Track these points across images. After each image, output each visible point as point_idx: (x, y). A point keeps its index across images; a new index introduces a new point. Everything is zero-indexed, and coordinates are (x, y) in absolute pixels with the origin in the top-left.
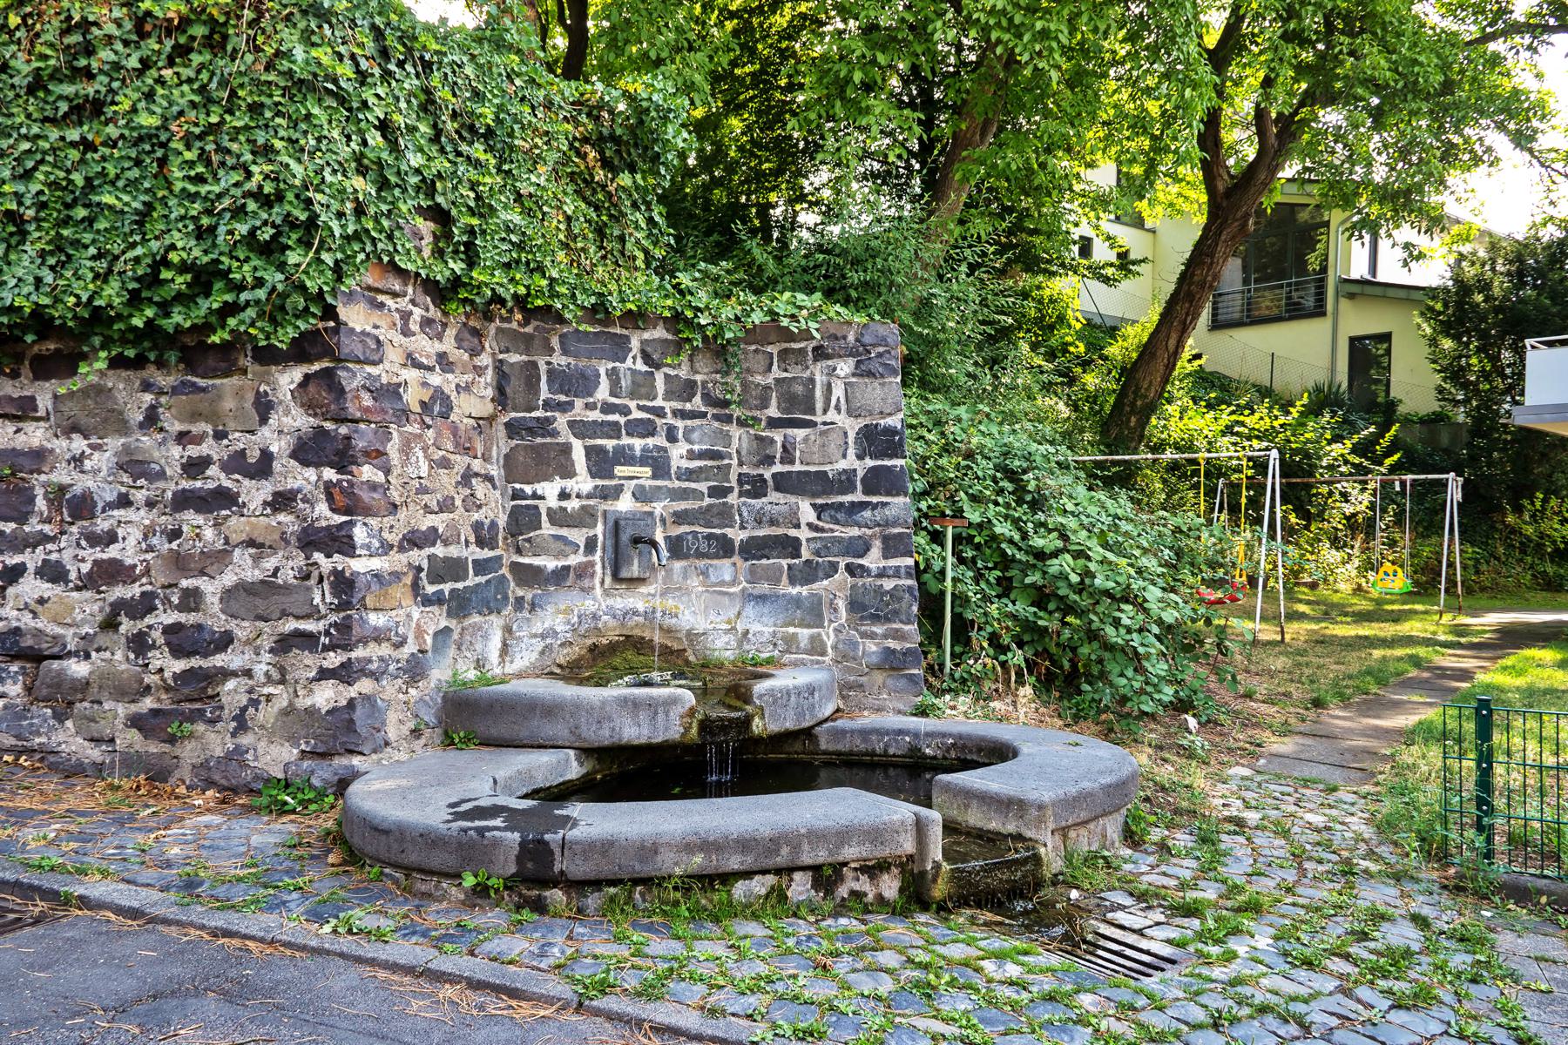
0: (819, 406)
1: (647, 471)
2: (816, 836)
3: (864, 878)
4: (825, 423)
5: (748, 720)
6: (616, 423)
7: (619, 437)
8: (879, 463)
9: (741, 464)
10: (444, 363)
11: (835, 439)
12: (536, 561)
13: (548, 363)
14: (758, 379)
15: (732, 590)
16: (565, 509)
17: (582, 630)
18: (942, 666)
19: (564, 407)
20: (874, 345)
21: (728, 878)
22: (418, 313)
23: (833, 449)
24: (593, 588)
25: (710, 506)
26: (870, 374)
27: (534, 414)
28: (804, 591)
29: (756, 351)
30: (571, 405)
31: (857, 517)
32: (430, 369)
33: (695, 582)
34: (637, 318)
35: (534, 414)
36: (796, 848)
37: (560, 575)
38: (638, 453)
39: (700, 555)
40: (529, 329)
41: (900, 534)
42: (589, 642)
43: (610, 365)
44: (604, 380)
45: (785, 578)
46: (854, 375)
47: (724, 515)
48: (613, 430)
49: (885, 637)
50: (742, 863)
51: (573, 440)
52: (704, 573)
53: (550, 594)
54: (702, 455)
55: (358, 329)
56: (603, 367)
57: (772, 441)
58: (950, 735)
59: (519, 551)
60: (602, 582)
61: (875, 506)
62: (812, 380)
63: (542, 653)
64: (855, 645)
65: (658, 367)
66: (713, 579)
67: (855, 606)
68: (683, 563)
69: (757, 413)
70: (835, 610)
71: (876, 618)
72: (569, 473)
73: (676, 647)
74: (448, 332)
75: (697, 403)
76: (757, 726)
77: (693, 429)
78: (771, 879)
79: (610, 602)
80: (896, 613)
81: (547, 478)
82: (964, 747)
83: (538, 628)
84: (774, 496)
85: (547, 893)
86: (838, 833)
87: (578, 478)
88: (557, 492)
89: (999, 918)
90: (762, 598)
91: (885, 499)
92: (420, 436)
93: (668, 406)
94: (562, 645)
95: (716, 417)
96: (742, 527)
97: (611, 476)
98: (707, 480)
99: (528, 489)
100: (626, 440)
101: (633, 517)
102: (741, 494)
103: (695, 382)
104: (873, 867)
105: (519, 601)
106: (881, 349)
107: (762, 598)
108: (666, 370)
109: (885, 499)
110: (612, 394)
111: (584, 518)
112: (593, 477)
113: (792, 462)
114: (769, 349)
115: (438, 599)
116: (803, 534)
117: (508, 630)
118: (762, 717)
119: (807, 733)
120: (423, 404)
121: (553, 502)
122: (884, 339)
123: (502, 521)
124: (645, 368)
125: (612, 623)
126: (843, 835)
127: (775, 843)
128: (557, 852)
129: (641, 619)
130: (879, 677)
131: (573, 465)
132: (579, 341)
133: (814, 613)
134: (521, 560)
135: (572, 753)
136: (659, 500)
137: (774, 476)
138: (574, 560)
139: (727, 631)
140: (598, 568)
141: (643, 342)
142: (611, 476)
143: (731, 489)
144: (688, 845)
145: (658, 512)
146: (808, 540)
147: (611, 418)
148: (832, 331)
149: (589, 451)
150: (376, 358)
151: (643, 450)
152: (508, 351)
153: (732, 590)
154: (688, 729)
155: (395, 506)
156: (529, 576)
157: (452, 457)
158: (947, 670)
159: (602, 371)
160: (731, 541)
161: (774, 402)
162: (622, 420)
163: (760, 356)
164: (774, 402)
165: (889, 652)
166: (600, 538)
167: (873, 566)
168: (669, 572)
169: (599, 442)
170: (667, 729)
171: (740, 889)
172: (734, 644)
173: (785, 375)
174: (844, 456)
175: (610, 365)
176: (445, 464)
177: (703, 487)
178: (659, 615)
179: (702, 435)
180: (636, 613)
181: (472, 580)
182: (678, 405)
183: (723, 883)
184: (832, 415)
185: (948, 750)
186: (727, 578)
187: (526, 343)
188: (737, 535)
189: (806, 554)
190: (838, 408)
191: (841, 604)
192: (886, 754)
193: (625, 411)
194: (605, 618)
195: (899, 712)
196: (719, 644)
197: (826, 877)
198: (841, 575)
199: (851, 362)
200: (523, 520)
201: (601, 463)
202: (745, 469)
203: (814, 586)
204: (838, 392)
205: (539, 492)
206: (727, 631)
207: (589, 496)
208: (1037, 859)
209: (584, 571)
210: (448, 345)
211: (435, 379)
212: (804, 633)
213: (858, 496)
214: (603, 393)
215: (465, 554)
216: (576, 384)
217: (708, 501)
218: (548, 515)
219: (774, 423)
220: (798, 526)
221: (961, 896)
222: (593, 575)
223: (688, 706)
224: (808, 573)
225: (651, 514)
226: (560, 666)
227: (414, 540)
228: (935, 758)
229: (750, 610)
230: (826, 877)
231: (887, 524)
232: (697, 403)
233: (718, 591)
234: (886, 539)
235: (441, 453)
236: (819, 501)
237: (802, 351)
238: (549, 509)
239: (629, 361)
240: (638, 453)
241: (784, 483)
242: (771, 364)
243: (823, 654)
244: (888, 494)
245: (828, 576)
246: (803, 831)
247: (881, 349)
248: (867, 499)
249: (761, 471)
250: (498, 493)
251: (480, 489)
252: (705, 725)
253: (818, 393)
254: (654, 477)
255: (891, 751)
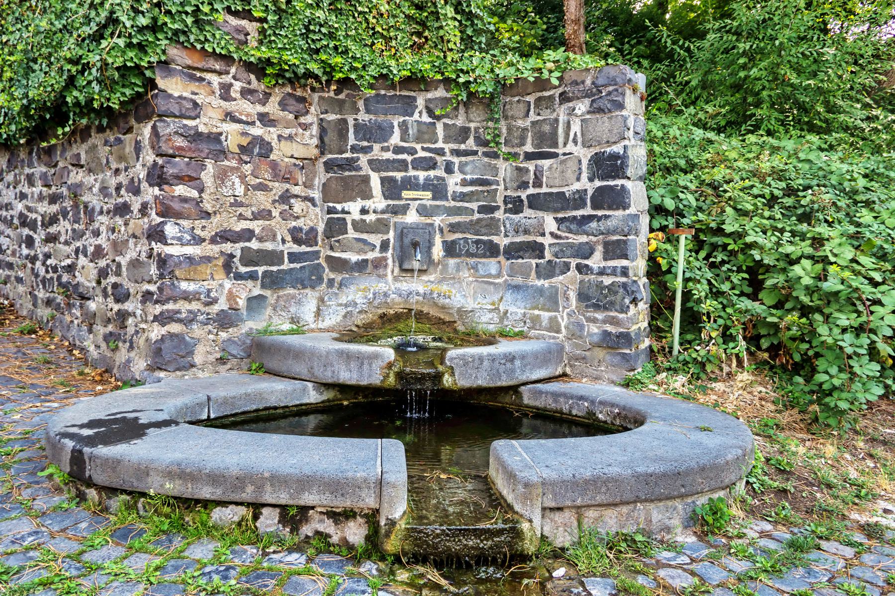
0: (561, 140)
1: (429, 194)
2: (278, 480)
3: (330, 522)
4: (564, 154)
5: (438, 377)
6: (404, 161)
7: (406, 171)
8: (605, 183)
9: (506, 189)
10: (265, 119)
11: (572, 165)
12: (344, 256)
13: (356, 120)
14: (520, 123)
15: (497, 281)
16: (365, 221)
17: (376, 303)
18: (671, 348)
19: (366, 150)
20: (605, 86)
21: (207, 504)
22: (238, 86)
23: (570, 175)
24: (386, 275)
25: (479, 220)
26: (600, 110)
27: (344, 156)
28: (545, 283)
29: (518, 101)
30: (370, 148)
31: (586, 228)
32: (253, 123)
33: (465, 274)
34: (416, 81)
35: (344, 156)
36: (260, 488)
37: (362, 265)
38: (421, 181)
39: (469, 255)
40: (342, 96)
41: (617, 240)
42: (380, 311)
43: (402, 119)
44: (396, 129)
45: (533, 273)
46: (589, 112)
47: (493, 226)
48: (402, 165)
49: (604, 322)
50: (212, 494)
51: (371, 173)
52: (475, 268)
53: (355, 278)
54: (472, 183)
55: (176, 94)
56: (396, 121)
57: (527, 170)
58: (617, 406)
59: (332, 248)
60: (393, 272)
61: (599, 219)
62: (556, 120)
63: (345, 316)
64: (581, 327)
65: (439, 118)
66: (481, 272)
67: (583, 296)
68: (457, 260)
69: (517, 150)
70: (567, 299)
71: (597, 307)
72: (367, 195)
73: (447, 319)
74: (272, 99)
75: (471, 144)
76: (447, 381)
77: (466, 163)
78: (242, 511)
79: (398, 285)
80: (612, 303)
81: (352, 199)
82: (626, 417)
83: (343, 300)
84: (528, 212)
85: (87, 491)
86: (299, 481)
87: (375, 200)
88: (359, 208)
89: (443, 582)
90: (517, 288)
91: (607, 213)
92: (238, 169)
93: (447, 147)
94: (360, 312)
95: (486, 154)
96: (506, 236)
97: (400, 198)
98: (478, 201)
99: (339, 207)
100: (412, 173)
101: (415, 228)
102: (506, 211)
103: (469, 129)
104: (339, 514)
105: (331, 282)
106: (611, 88)
107: (517, 288)
108: (446, 121)
109: (607, 213)
110: (402, 140)
111: (380, 226)
112: (386, 198)
113: (540, 186)
114: (528, 98)
115: (252, 276)
116: (547, 241)
117: (321, 300)
118: (453, 374)
119: (514, 389)
120: (241, 147)
121: (356, 216)
122: (614, 80)
123: (321, 227)
124: (430, 120)
125: (398, 299)
126: (304, 483)
127: (241, 481)
128: (87, 461)
129: (421, 298)
130: (600, 353)
131: (371, 190)
132: (378, 102)
133: (552, 300)
134: (333, 254)
135: (310, 385)
136: (438, 215)
137: (528, 197)
138: (370, 256)
139: (491, 311)
140: (390, 261)
141: (428, 101)
142: (400, 198)
143: (498, 208)
144: (170, 472)
145: (436, 224)
146: (550, 245)
147: (400, 157)
148: (574, 78)
149: (383, 180)
150: (193, 114)
151: (426, 179)
152: (326, 112)
153: (497, 281)
154: (387, 376)
155: (209, 214)
156: (338, 265)
157: (270, 184)
158: (675, 352)
159: (396, 124)
160: (497, 246)
161: (529, 140)
162: (409, 158)
163: (521, 105)
164: (529, 140)
165: (606, 334)
166: (392, 241)
167: (595, 267)
168: (445, 266)
169: (391, 174)
170: (370, 376)
171: (218, 514)
172: (497, 320)
173: (539, 118)
174: (578, 179)
175: (402, 119)
176: (262, 187)
177: (474, 206)
178: (435, 295)
179: (475, 167)
180: (418, 294)
181: (286, 265)
182: (455, 146)
183: (205, 507)
184: (570, 147)
185: (614, 418)
186: (494, 272)
187: (340, 106)
188: (502, 241)
189: (548, 255)
190: (575, 142)
191: (573, 296)
192: (570, 414)
193: (412, 152)
194: (394, 296)
195: (613, 382)
196: (484, 319)
197: (293, 517)
198: (573, 273)
199: (587, 101)
200: (335, 227)
201: (392, 189)
202: (509, 193)
203: (554, 280)
204: (576, 127)
205: (346, 209)
206: (491, 311)
207: (383, 212)
208: (517, 534)
209: (379, 264)
210: (272, 107)
211: (257, 131)
212: (545, 315)
213: (588, 211)
214: (395, 139)
215: (281, 247)
216: (374, 133)
217: (477, 216)
218: (352, 224)
219: (529, 157)
220: (543, 235)
221: (415, 556)
222: (386, 266)
223: (387, 361)
224: (548, 271)
225: (432, 225)
226: (357, 326)
227: (224, 236)
228: (605, 422)
229: (509, 296)
230: (293, 517)
231: (609, 232)
232: (471, 144)
233: (485, 282)
234: (606, 244)
235: (258, 181)
236: (560, 215)
237: (551, 98)
238: (353, 220)
239: (416, 116)
240: (421, 181)
241: (535, 202)
242: (529, 110)
243: (558, 331)
244: (610, 208)
245: (563, 273)
246: (266, 475)
247: (611, 88)
248: (594, 213)
249: (519, 194)
250: (318, 210)
251: (298, 206)
252: (400, 376)
253: (561, 130)
254: (434, 198)
255: (574, 412)
